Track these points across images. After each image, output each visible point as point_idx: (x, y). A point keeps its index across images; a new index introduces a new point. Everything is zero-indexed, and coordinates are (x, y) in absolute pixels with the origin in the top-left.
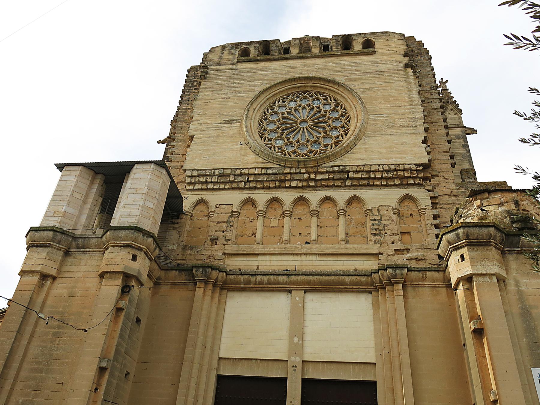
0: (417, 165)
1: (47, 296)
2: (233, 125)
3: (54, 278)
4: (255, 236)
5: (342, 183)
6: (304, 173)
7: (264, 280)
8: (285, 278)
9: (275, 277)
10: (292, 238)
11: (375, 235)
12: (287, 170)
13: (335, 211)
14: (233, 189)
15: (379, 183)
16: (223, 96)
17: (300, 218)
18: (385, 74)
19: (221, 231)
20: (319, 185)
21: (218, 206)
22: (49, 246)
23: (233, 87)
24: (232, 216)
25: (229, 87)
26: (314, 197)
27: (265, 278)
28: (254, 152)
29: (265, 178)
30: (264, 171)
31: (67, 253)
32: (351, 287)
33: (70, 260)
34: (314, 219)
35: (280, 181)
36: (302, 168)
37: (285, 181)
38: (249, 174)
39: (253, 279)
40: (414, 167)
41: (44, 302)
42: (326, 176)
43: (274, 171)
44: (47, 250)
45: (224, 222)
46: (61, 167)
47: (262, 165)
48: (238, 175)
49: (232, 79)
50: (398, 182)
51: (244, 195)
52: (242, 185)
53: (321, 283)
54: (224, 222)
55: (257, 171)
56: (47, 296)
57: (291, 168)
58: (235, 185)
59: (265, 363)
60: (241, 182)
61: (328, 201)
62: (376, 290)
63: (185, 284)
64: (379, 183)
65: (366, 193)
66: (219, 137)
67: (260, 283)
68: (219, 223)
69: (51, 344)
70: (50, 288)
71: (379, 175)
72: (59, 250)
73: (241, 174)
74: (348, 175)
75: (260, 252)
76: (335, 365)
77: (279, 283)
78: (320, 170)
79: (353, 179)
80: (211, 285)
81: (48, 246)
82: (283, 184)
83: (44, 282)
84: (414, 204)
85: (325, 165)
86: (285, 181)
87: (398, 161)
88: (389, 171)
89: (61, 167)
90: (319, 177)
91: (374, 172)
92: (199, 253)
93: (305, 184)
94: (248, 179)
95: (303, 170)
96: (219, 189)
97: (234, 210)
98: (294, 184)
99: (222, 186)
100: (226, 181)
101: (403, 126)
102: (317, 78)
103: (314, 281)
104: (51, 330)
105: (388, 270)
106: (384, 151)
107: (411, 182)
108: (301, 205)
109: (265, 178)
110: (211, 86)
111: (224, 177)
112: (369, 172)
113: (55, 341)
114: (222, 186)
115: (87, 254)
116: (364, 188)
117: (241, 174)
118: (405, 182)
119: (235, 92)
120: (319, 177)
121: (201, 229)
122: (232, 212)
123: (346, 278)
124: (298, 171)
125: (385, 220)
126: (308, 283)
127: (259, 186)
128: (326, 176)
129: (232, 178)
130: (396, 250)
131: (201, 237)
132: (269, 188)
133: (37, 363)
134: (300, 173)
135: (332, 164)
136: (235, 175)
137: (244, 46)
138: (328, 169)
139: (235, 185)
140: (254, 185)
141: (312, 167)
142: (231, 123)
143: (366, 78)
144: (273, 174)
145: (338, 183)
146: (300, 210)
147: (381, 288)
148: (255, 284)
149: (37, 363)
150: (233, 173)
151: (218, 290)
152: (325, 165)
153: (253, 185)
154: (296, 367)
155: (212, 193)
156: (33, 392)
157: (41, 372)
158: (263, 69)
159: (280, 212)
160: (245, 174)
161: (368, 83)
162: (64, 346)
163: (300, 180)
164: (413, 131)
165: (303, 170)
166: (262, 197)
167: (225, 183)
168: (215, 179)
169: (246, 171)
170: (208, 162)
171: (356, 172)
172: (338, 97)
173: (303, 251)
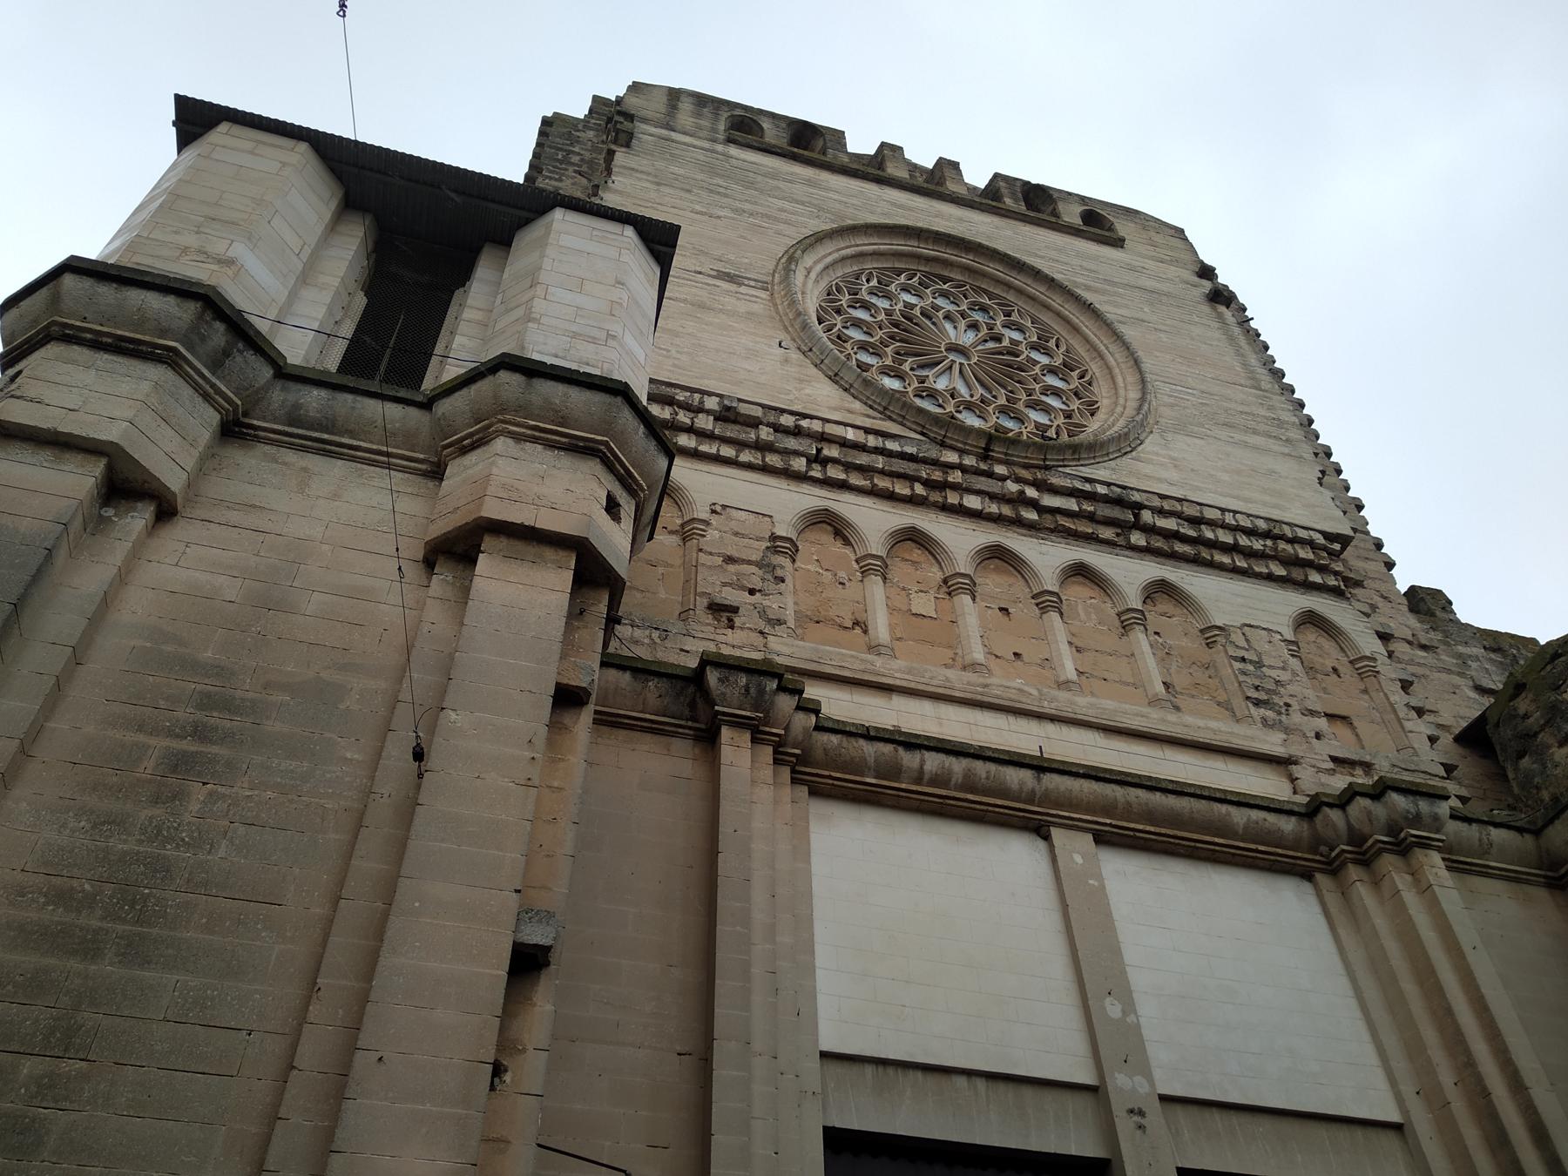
0: (1326, 535)
1: (122, 578)
2: (743, 289)
3: (166, 511)
4: (865, 632)
5: (1118, 535)
6: (1003, 479)
7: (950, 772)
8: (1026, 776)
9: (992, 767)
10: (993, 664)
11: (1257, 703)
12: (951, 457)
13: (1113, 612)
14: (765, 469)
15: (1226, 560)
16: (698, 207)
17: (1004, 610)
18: (1164, 299)
19: (743, 588)
20: (1052, 526)
21: (718, 509)
22: (170, 359)
23: (726, 196)
24: (775, 550)
25: (711, 191)
26: (1047, 557)
27: (958, 766)
28: (834, 378)
29: (880, 462)
30: (872, 441)
31: (234, 430)
32: (1253, 846)
33: (250, 461)
34: (1139, 635)
35: (927, 483)
36: (1000, 462)
37: (943, 486)
38: (823, 438)
39: (910, 759)
40: (1320, 539)
41: (106, 602)
42: (1071, 504)
43: (910, 450)
44: (157, 373)
45: (749, 562)
46: (195, 120)
47: (868, 423)
48: (786, 431)
49: (718, 175)
50: (1280, 571)
51: (811, 498)
52: (799, 464)
53: (1150, 816)
54: (749, 562)
55: (851, 434)
56: (122, 578)
57: (962, 452)
58: (773, 460)
59: (1006, 1091)
60: (797, 453)
61: (1081, 579)
62: (1334, 869)
63: (654, 729)
64: (1226, 560)
65: (1195, 581)
66: (702, 306)
67: (936, 781)
68: (730, 560)
69: (158, 811)
70: (134, 556)
71: (1226, 537)
72: (206, 397)
73: (797, 432)
74: (1137, 516)
75: (898, 683)
76: (1266, 1124)
77: (1004, 792)
78: (1055, 480)
79: (1150, 530)
80: (770, 749)
81: (159, 360)
82: (935, 497)
83: (109, 512)
84: (1333, 644)
85: (1067, 470)
86: (943, 486)
87: (1275, 514)
88: (1251, 532)
89: (195, 120)
90: (1050, 501)
91: (1212, 524)
92: (668, 644)
93: (1007, 511)
94: (819, 451)
95: (1000, 469)
96: (717, 459)
97: (781, 532)
98: (973, 502)
99: (727, 451)
100: (743, 436)
101: (1255, 432)
102: (988, 248)
103: (1129, 803)
104: (153, 741)
105: (1395, 797)
106: (1225, 477)
107: (1315, 577)
108: (997, 570)
109: (880, 462)
110: (650, 170)
111: (737, 427)
112: (1196, 521)
113: (179, 796)
114: (727, 451)
115: (339, 456)
116: (1184, 565)
117: (797, 432)
118: (1297, 574)
119: (735, 210)
120: (1050, 501)
121: (660, 570)
122: (774, 538)
123: (1233, 810)
124: (983, 466)
125: (1270, 667)
126: (1108, 809)
127: (856, 480)
128: (1071, 504)
129: (765, 433)
130: (1334, 759)
131: (663, 595)
132: (890, 496)
133: (61, 897)
134: (990, 475)
135: (1086, 472)
136: (778, 428)
137: (738, 112)
138: (1078, 485)
139: (773, 460)
140: (842, 476)
141: (1026, 467)
142: (740, 284)
143: (1120, 295)
144: (903, 456)
145: (1107, 533)
146: (994, 583)
147: (1356, 862)
148: (919, 780)
149: (61, 897)
150: (772, 419)
151: (1353, 872)
152: (1067, 470)
153: (835, 473)
154: (1141, 1113)
155: (689, 465)
156: (27, 1067)
157: (89, 948)
158: (810, 183)
159: (935, 575)
160: (810, 435)
161: (1126, 306)
162: (242, 830)
163: (993, 497)
164: (1286, 451)
165: (1000, 469)
166: (875, 521)
167: (741, 445)
168: (706, 422)
169: (816, 426)
170: (675, 365)
171: (1161, 512)
172: (1046, 318)
173: (1048, 708)
